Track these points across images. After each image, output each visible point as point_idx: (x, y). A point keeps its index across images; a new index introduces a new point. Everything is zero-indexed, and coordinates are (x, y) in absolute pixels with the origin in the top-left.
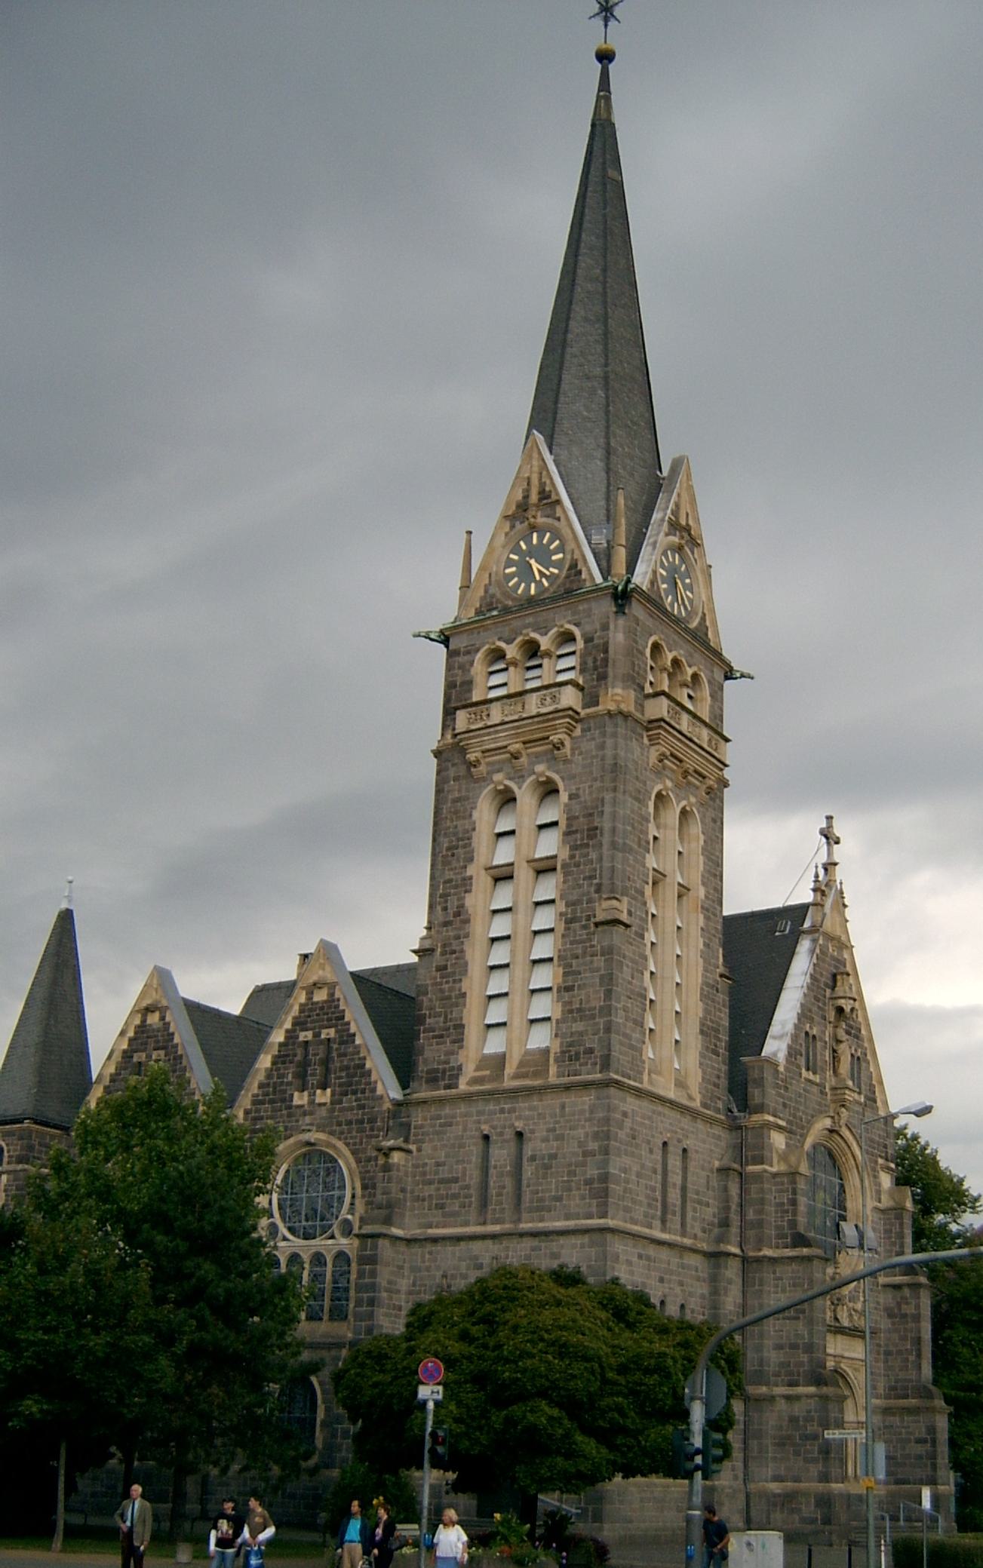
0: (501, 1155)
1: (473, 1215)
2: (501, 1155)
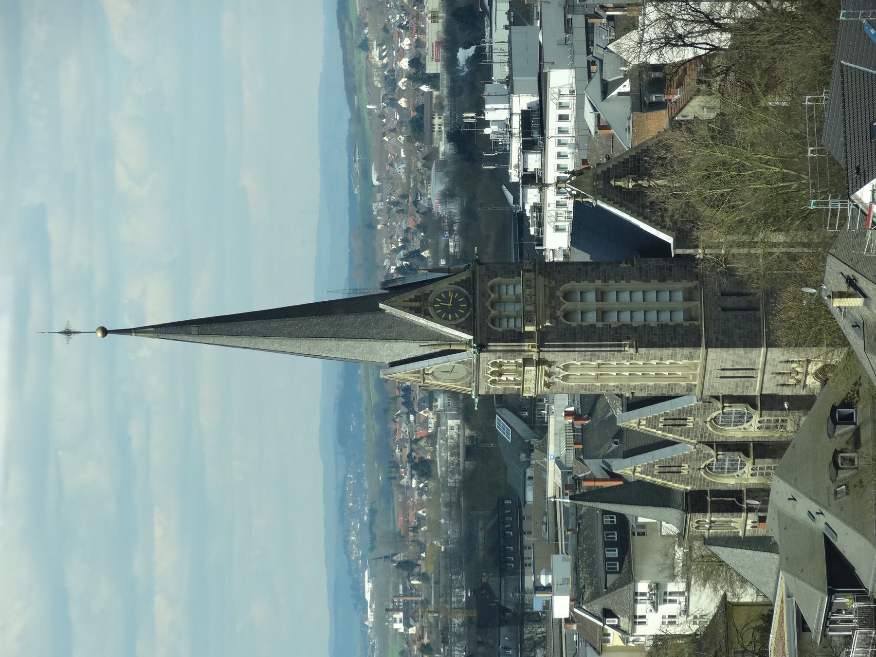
1: (757, 313)
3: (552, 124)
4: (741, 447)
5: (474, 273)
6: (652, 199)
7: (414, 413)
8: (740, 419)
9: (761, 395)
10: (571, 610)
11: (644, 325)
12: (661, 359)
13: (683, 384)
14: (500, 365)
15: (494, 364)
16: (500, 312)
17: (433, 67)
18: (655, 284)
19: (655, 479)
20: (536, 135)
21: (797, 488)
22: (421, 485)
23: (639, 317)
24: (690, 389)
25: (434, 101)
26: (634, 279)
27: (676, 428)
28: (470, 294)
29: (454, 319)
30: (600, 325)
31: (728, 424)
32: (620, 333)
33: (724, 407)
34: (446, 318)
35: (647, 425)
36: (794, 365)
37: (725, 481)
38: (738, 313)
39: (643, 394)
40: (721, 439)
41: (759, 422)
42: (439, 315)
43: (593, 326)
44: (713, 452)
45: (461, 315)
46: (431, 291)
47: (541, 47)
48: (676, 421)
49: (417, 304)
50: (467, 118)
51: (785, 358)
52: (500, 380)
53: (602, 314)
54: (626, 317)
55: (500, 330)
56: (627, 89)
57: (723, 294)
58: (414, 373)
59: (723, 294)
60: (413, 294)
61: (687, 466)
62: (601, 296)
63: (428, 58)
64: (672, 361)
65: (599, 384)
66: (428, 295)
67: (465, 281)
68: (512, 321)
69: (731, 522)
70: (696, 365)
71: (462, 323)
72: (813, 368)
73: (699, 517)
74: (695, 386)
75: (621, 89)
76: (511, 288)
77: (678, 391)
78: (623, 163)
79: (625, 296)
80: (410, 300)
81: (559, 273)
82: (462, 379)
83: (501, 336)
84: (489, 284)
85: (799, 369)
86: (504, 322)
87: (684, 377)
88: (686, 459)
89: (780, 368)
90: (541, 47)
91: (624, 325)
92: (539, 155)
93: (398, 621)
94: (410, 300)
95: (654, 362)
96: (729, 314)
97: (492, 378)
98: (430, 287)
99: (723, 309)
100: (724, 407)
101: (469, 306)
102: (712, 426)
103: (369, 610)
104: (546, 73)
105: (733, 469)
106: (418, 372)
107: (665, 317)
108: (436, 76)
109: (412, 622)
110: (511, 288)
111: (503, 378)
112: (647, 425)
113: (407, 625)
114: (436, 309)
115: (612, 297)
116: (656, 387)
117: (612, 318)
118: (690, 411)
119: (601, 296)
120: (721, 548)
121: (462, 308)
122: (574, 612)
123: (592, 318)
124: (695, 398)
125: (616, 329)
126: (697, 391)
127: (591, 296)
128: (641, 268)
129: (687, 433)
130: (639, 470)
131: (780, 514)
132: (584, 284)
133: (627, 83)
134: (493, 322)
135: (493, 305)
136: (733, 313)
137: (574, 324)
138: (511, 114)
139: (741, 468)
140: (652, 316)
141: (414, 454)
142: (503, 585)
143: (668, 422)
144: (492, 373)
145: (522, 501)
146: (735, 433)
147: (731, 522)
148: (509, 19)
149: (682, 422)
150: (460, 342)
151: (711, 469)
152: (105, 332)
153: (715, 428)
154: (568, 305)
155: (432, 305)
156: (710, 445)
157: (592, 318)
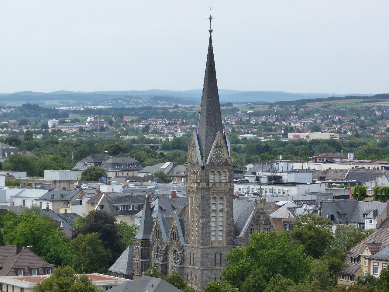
0: (218, 257)
2: (218, 257)
3: (277, 188)
4: (166, 259)
5: (230, 165)
6: (183, 140)
7: (166, 126)
8: (175, 259)
9: (184, 267)
10: (104, 193)
11: (210, 226)
12: (198, 232)
13: (189, 240)
14: (197, 174)
15: (197, 172)
16: (216, 174)
17: (291, 135)
18: (225, 230)
19: (154, 228)
20: (273, 181)
21: (156, 287)
22: (140, 128)
23: (213, 224)
24: (187, 242)
25: (279, 136)
26: (227, 222)
27: (173, 236)
28: (223, 164)
29: (214, 158)
30: (211, 210)
31: (174, 255)
32: (207, 217)
33: (180, 254)
34: (214, 155)
35: (174, 226)
36: (195, 279)
37: (153, 253)
38: (214, 259)
39: (185, 225)
40: (168, 252)
41: (174, 266)
42: (215, 152)
43: (210, 208)
44: (163, 249)
45: (215, 160)
46: (224, 150)
47: (305, 184)
48: (175, 236)
49: (219, 145)
50: (280, 157)
51: (197, 275)
52: (191, 174)
53: (215, 211)
54: (213, 219)
55: (209, 174)
56: (291, 217)
57: (221, 254)
58: (194, 143)
59: (221, 254)
60: (223, 143)
61: (159, 240)
62: (221, 211)
63: (294, 133)
64: (197, 236)
65: (189, 209)
66: (222, 149)
67: (227, 162)
68: (212, 178)
69: (138, 256)
70: (195, 244)
71: (212, 161)
72: (194, 286)
73: (140, 243)
74: (188, 244)
75: (291, 214)
76: (224, 178)
77: (186, 237)
78: (268, 219)
79: (221, 219)
80: (221, 142)
81: (230, 196)
82: (192, 160)
83: (207, 174)
84: (226, 170)
85: (193, 281)
86: (212, 176)
87: (191, 240)
88: (161, 239)
89: (194, 274)
90: (305, 184)
91: (210, 219)
92: (266, 182)
93: (91, 119)
94: (221, 142)
95: (197, 229)
96: (213, 257)
97: (192, 171)
98: (225, 148)
99: (215, 254)
100: (180, 254)
101: (219, 163)
102: (173, 249)
103: (94, 107)
104: (295, 186)
105: (157, 256)
106: (195, 144)
107: (213, 233)
108: (287, 137)
109: (90, 124)
110: (224, 178)
111: (192, 175)
112: (174, 226)
113: (90, 122)
114: (217, 151)
115: (221, 214)
116: (188, 229)
117: (213, 214)
118: (179, 241)
119: (221, 211)
120: (128, 251)
121: (217, 161)
122: (102, 194)
123: (213, 207)
124: (183, 243)
125: (209, 216)
126: (185, 245)
127: (221, 207)
128: (231, 225)
129: (171, 240)
130: (157, 222)
131: (148, 281)
132: (226, 204)
133: (293, 217)
134: (213, 172)
135: (219, 172)
136: (214, 258)
137: (211, 201)
138: (281, 172)
139: (157, 259)
140: (213, 229)
141: (151, 125)
142: (110, 164)
143: (175, 234)
144: (194, 171)
145: (139, 171)
146: (171, 257)
147: (138, 256)
148: (313, 170)
149: (175, 239)
150: (206, 160)
151: (157, 248)
152: (211, 31)
153: (172, 251)
154: (218, 198)
155: (219, 150)
156: (166, 248)
157: (213, 207)
